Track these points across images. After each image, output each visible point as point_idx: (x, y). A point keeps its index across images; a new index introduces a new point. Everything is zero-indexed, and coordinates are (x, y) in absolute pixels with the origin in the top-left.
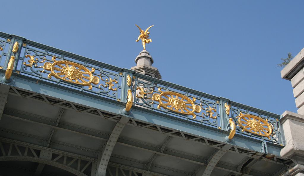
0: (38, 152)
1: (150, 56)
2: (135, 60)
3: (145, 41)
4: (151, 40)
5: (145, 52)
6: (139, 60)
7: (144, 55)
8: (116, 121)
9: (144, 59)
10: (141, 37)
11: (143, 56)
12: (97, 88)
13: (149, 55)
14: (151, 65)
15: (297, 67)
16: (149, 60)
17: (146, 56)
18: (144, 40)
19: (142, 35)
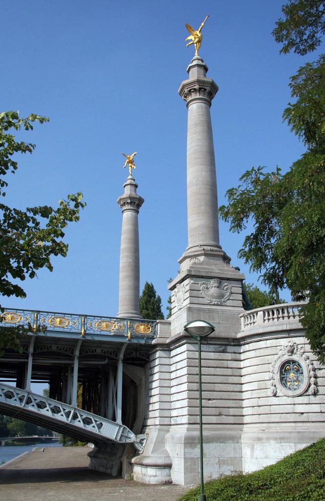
0: (51, 347)
1: (204, 64)
2: (187, 70)
3: (131, 166)
4: (135, 167)
5: (131, 179)
6: (126, 187)
7: (196, 63)
8: (30, 272)
9: (129, 186)
10: (128, 162)
11: (128, 183)
12: (223, 398)
13: (202, 61)
14: (205, 76)
15: (63, 358)
16: (134, 186)
17: (199, 64)
18: (130, 164)
19: (128, 160)
